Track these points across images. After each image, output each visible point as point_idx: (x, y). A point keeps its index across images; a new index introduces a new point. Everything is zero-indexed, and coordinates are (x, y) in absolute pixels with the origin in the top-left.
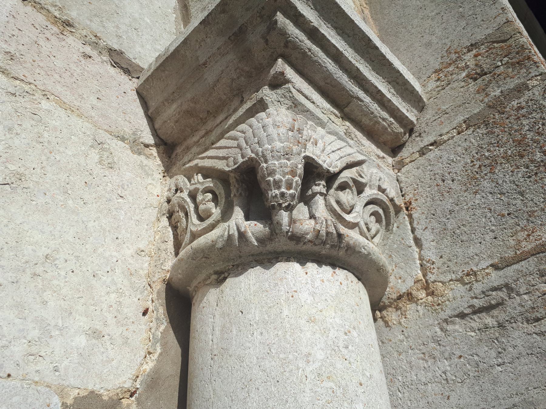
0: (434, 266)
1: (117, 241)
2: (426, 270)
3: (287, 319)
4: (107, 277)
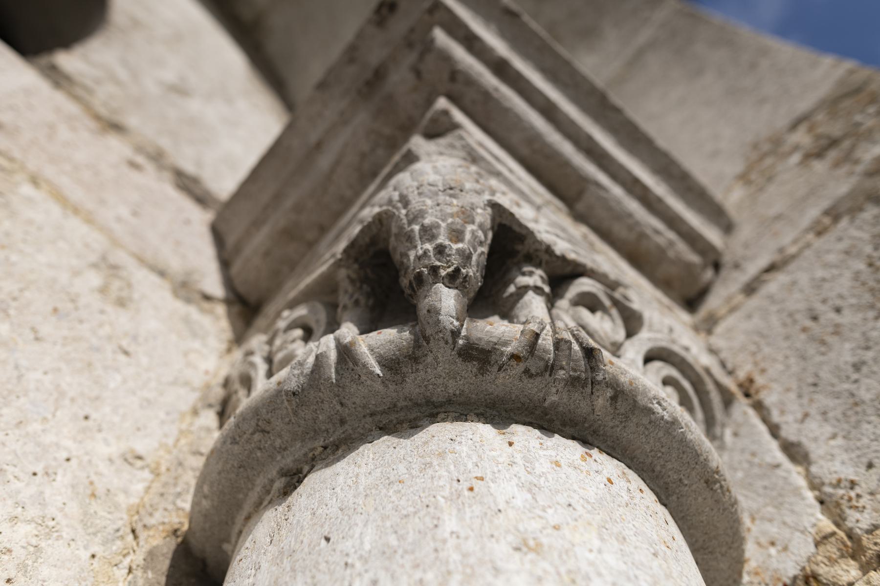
0: (858, 490)
1: (85, 423)
2: (838, 505)
3: (452, 542)
4: (28, 485)
